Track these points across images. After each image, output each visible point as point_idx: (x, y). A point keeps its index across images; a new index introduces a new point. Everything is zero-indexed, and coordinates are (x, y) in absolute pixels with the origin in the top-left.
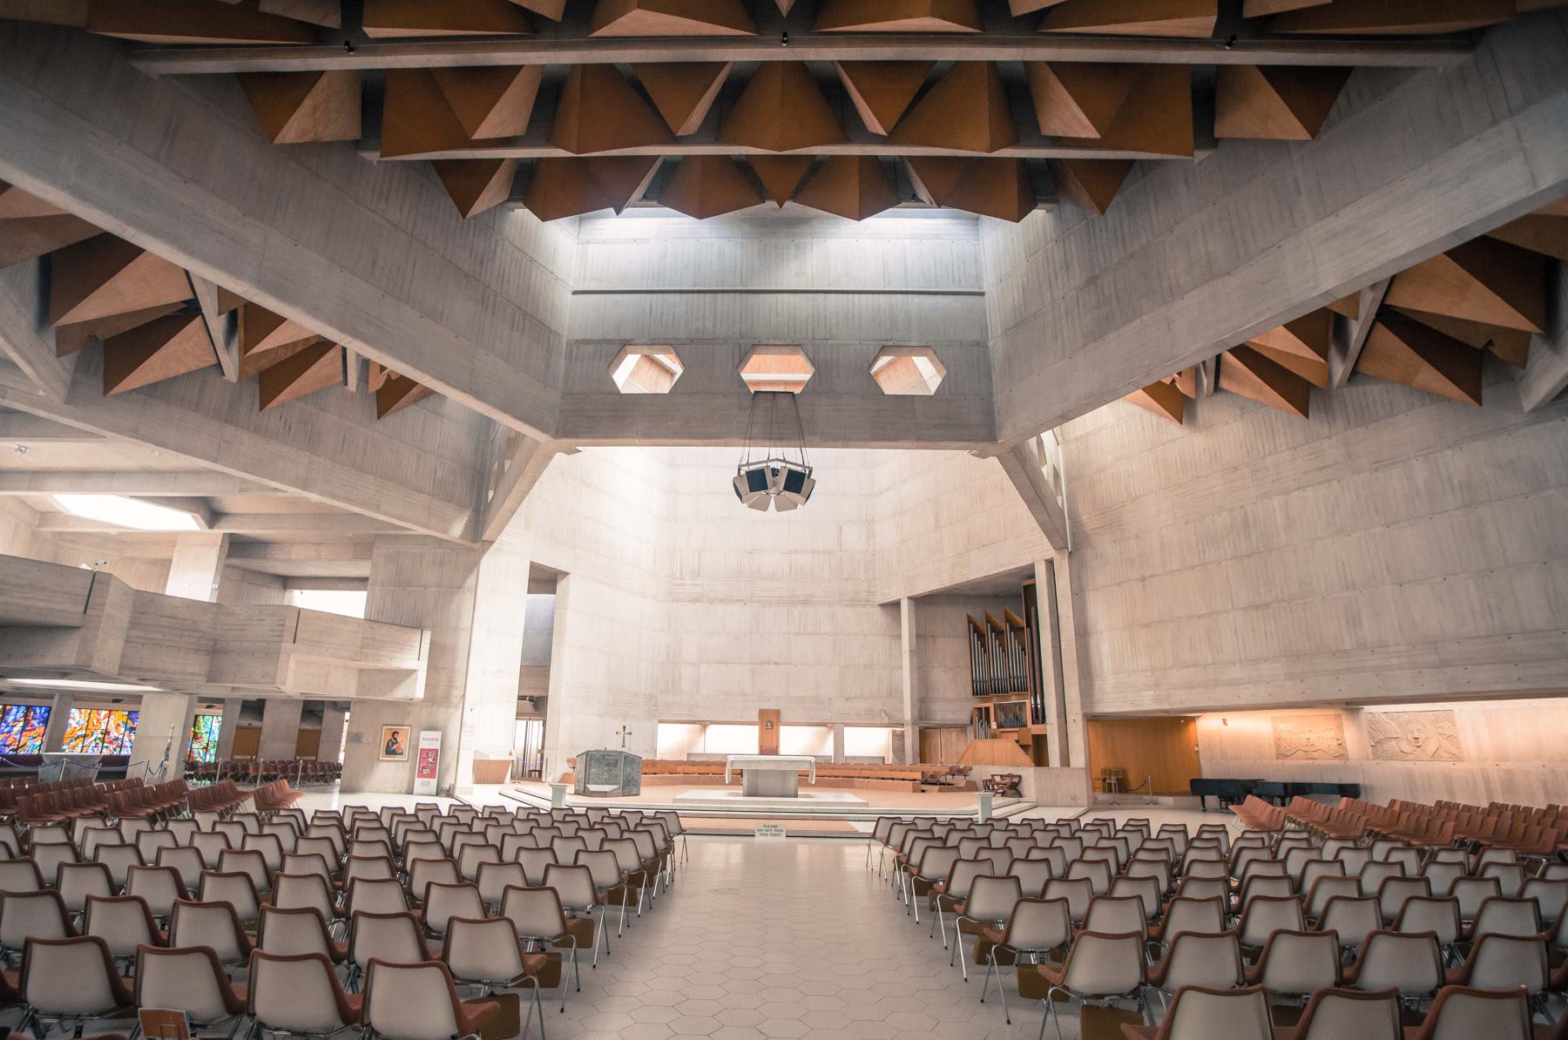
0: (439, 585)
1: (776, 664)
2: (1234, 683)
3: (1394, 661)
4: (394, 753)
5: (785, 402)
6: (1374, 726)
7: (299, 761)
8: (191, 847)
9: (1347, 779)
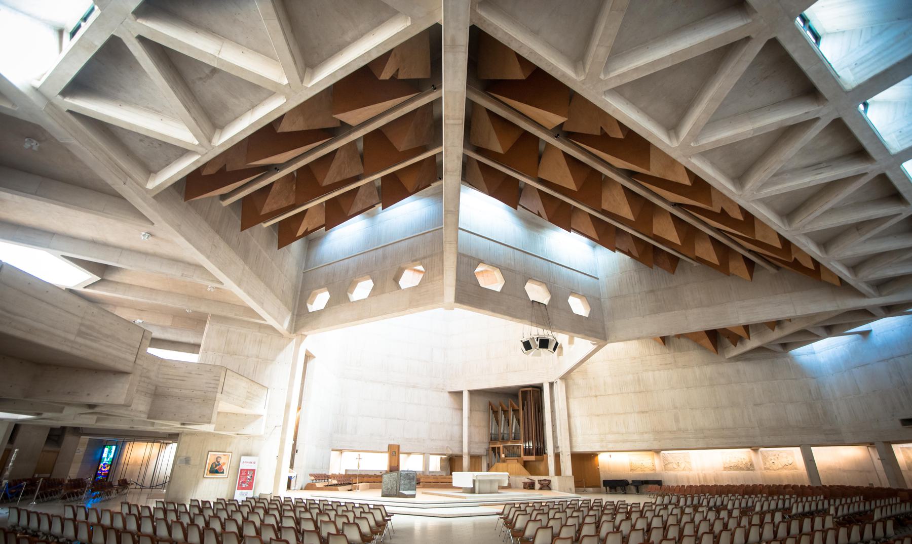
0: (257, 357)
1: (398, 419)
2: (634, 441)
3: (690, 436)
4: (217, 472)
5: (543, 308)
6: (665, 459)
7: (39, 478)
8: (354, 523)
9: (659, 479)
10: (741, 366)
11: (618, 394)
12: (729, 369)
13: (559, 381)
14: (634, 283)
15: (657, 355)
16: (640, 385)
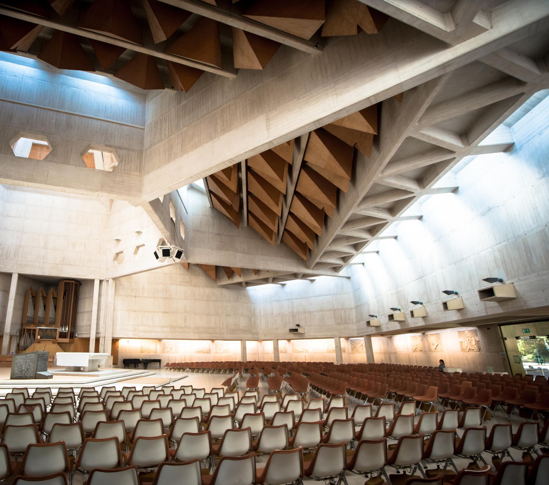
2: (157, 332)
3: (191, 331)
6: (164, 345)
9: (158, 358)
10: (225, 291)
11: (151, 297)
12: (218, 292)
13: (111, 281)
14: (209, 225)
15: (181, 275)
16: (166, 293)
